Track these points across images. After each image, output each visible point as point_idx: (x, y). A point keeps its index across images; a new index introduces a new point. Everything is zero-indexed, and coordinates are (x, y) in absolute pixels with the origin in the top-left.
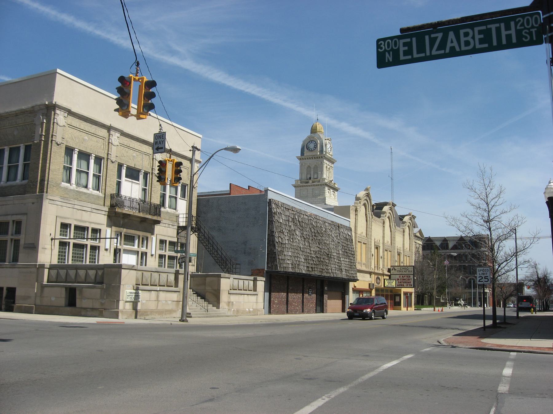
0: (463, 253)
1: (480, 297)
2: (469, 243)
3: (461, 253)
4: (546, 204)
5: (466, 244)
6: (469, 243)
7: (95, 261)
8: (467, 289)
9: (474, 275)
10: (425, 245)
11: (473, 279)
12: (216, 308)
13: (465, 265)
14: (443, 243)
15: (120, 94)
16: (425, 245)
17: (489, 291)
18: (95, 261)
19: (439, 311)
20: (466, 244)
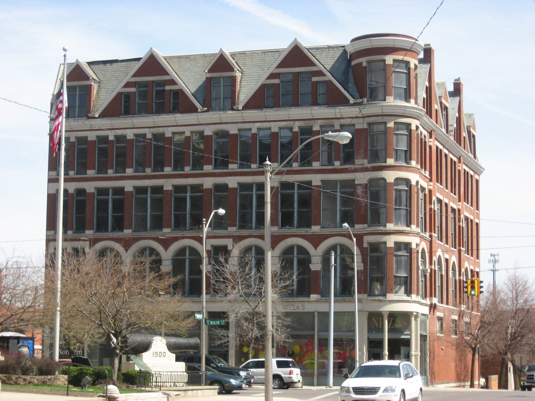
0: (298, 124)
1: (375, 336)
2: (329, 77)
3: (309, 123)
4: (48, 136)
5: (314, 79)
6: (329, 77)
7: (189, 189)
8: (317, 301)
9: (303, 231)
10: (133, 90)
11: (302, 250)
12: (89, 139)
13: (122, 189)
14: (211, 78)
15: (182, 361)
16: (133, 90)
17: (425, 310)
18: (189, 189)
19: (170, 386)
20: (314, 79)
